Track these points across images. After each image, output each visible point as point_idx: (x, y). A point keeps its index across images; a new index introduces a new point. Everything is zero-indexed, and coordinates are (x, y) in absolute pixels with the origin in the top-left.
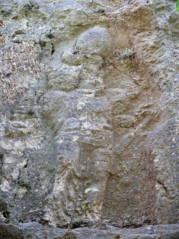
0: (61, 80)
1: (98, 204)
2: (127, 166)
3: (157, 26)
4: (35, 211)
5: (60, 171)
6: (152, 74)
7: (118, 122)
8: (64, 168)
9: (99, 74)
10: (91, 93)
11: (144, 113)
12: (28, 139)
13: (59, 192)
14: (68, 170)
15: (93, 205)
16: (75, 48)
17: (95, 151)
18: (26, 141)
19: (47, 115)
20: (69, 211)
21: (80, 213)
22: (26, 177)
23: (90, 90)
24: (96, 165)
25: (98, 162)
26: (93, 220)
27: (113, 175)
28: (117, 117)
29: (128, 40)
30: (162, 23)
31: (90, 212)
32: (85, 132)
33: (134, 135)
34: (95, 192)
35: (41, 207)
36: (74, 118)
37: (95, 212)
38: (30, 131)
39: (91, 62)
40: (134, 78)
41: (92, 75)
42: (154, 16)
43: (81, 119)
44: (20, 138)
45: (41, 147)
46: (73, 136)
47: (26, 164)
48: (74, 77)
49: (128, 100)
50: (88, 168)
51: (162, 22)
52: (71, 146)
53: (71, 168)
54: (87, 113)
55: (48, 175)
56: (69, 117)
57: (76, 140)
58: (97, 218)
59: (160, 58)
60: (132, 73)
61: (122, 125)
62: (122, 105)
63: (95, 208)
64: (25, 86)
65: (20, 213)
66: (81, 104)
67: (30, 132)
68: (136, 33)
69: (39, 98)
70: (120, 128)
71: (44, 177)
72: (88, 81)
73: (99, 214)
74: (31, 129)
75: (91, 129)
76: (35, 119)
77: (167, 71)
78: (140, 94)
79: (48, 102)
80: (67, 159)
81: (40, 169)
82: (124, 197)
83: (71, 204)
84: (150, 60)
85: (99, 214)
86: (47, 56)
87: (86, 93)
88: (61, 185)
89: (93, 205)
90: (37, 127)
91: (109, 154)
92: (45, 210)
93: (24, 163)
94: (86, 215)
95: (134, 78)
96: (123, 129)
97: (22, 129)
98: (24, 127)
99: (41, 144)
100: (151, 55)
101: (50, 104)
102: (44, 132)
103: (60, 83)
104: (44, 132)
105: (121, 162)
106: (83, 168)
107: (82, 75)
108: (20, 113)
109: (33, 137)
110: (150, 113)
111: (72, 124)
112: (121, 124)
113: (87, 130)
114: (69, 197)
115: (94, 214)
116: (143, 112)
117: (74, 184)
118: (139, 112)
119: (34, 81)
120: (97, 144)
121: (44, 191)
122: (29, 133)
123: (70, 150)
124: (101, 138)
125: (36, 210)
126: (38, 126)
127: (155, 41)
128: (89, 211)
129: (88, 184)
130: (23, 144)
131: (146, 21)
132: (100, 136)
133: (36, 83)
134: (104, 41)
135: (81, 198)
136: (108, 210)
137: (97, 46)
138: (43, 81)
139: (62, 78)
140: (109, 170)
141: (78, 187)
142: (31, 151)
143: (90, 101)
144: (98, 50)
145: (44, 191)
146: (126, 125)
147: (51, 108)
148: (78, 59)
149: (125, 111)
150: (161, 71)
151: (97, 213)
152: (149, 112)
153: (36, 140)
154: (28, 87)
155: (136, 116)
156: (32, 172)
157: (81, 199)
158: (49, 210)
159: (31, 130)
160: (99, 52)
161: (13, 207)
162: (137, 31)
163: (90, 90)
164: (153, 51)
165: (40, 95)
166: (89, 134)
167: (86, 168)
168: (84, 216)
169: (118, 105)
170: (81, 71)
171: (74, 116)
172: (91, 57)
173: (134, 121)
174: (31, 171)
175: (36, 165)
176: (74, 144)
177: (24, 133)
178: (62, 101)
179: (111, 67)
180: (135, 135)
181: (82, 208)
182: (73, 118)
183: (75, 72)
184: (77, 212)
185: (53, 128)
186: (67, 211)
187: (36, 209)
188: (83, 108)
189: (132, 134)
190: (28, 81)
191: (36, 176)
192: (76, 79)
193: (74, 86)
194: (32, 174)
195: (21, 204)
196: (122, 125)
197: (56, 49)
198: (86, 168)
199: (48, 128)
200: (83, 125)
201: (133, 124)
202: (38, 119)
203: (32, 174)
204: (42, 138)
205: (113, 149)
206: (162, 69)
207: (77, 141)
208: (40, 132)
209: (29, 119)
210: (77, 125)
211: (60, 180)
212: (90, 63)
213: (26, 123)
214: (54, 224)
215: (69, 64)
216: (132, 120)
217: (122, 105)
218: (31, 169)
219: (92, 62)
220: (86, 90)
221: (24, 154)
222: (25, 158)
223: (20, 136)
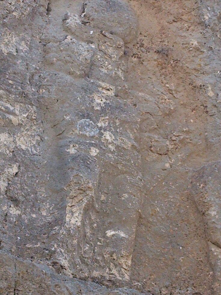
1: (128, 256)
2: (162, 209)
4: (36, 246)
5: (75, 195)
6: (195, 87)
8: (82, 192)
9: (120, 64)
10: (108, 90)
11: (184, 139)
12: (19, 135)
13: (75, 226)
14: (87, 197)
15: (121, 257)
16: (82, 16)
17: (119, 176)
18: (15, 136)
19: (46, 104)
20: (86, 258)
21: (102, 264)
23: (108, 85)
24: (123, 198)
25: (125, 194)
27: (142, 219)
28: (146, 134)
29: (160, 28)
30: (209, 18)
31: (116, 266)
32: (107, 146)
33: (170, 167)
35: (44, 243)
36: (91, 120)
38: (21, 123)
40: (168, 85)
41: (110, 64)
42: (199, 5)
43: (99, 125)
44: (6, 128)
45: (37, 151)
46: (92, 148)
47: (17, 171)
49: (161, 114)
50: (110, 200)
54: (107, 117)
55: (50, 196)
57: (95, 154)
58: (127, 277)
59: (207, 68)
60: (164, 77)
61: (152, 149)
62: (153, 119)
63: (122, 261)
64: (11, 50)
66: (99, 101)
68: (172, 21)
69: (33, 75)
70: (150, 153)
71: (44, 197)
72: (104, 71)
73: (128, 271)
74: (23, 119)
75: (115, 144)
76: (30, 106)
78: (175, 111)
81: (37, 184)
83: (87, 248)
84: (193, 67)
85: (128, 271)
86: (41, 14)
87: (103, 88)
88: (76, 217)
89: (121, 257)
91: (139, 187)
92: (53, 249)
93: (15, 170)
94: (110, 270)
95: (168, 85)
96: (154, 155)
97: (11, 117)
98: (14, 114)
99: (36, 146)
101: (53, 89)
102: (41, 129)
103: (67, 62)
104: (41, 129)
106: (103, 198)
107: (96, 59)
108: (7, 90)
109: (26, 132)
110: (191, 142)
112: (151, 147)
113: (110, 143)
114: (85, 236)
115: (123, 270)
116: (182, 137)
118: (176, 136)
119: (23, 47)
120: (124, 168)
122: (20, 125)
124: (129, 161)
125: (38, 246)
126: (33, 118)
127: (200, 40)
128: (114, 264)
130: (12, 139)
131: (186, 9)
132: (128, 157)
133: (26, 51)
135: (101, 242)
136: (137, 269)
137: (119, 23)
138: (37, 51)
139: (70, 56)
140: (140, 211)
141: (95, 225)
142: (24, 153)
145: (46, 219)
146: (158, 150)
147: (54, 96)
148: (91, 33)
149: (155, 128)
150: (209, 85)
151: (125, 269)
152: (191, 140)
153: (29, 139)
154: (16, 53)
157: (100, 244)
158: (63, 251)
159: (23, 121)
160: (121, 33)
161: (6, 233)
163: (107, 86)
164: (196, 54)
165: (34, 71)
167: (107, 200)
168: (108, 270)
169: (148, 118)
170: (95, 54)
171: (88, 116)
172: (111, 38)
173: (170, 147)
174: (25, 184)
175: (32, 177)
176: (93, 160)
177: (12, 123)
178: (70, 90)
179: (135, 60)
180: (171, 167)
181: (103, 257)
182: (89, 120)
184: (97, 261)
186: (83, 257)
187: (113, 235)
189: (167, 165)
190: (15, 44)
191: (33, 194)
193: (85, 72)
194: (27, 190)
195: (14, 231)
196: (152, 149)
197: (53, 7)
198: (107, 200)
200: (104, 135)
201: (168, 151)
202: (34, 107)
203: (27, 190)
205: (142, 180)
206: (211, 84)
207: (96, 156)
208: (34, 127)
210: (94, 132)
211: (74, 209)
212: (107, 44)
213: (17, 109)
214: (69, 272)
216: (167, 145)
218: (25, 181)
219: (111, 44)
220: (103, 84)
221: (14, 155)
222: (16, 161)
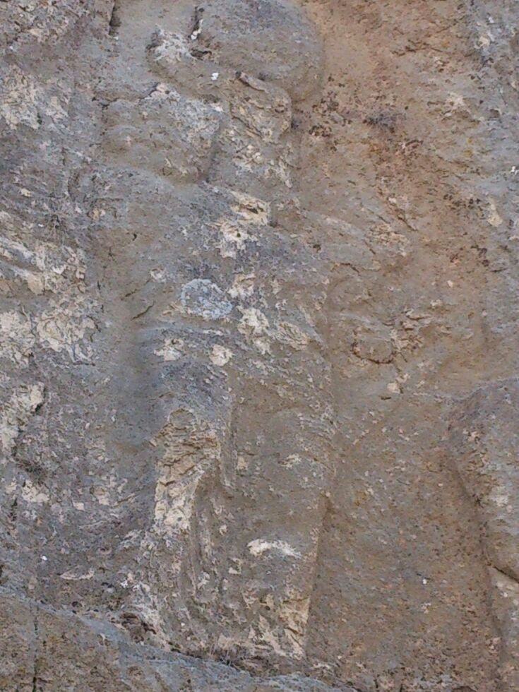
0: (159, 137)
3: (476, 47)
4: (83, 577)
5: (175, 457)
6: (457, 204)
7: (347, 334)
8: (191, 450)
10: (254, 211)
11: (431, 326)
12: (44, 316)
14: (205, 462)
19: (109, 244)
20: (201, 605)
21: (239, 619)
22: (45, 449)
23: (254, 200)
24: (289, 466)
25: (294, 456)
26: (283, 654)
27: (334, 513)
28: (344, 315)
29: (375, 65)
30: (491, 42)
34: (289, 556)
36: (213, 282)
37: (290, 626)
38: (50, 287)
39: (256, 103)
40: (393, 200)
41: (258, 150)
42: (468, 13)
44: (14, 301)
45: (86, 355)
46: (216, 347)
47: (39, 401)
48: (202, 139)
49: (378, 267)
50: (258, 469)
51: (493, 40)
52: (209, 378)
53: (213, 457)
55: (118, 460)
56: (195, 273)
57: (224, 362)
59: (486, 159)
60: (385, 181)
61: (358, 349)
62: (359, 280)
63: (287, 612)
64: (26, 118)
65: (438, 621)
66: (231, 237)
67: (51, 291)
68: (403, 49)
70: (353, 359)
72: (245, 165)
73: (302, 635)
74: (54, 280)
75: (271, 338)
76: (69, 249)
77: (512, 207)
78: (411, 259)
79: (113, 200)
80: (202, 421)
81: (88, 432)
82: (372, 595)
83: (204, 582)
85: (302, 635)
86: (97, 34)
87: (242, 207)
88: (179, 508)
89: (284, 602)
90: (75, 280)
91: (327, 439)
93: (35, 398)
94: (259, 633)
95: (393, 200)
96: (362, 363)
97: (26, 274)
98: (33, 268)
99: (85, 341)
100: (456, 137)
101: (125, 209)
102: (96, 304)
103: (156, 146)
104: (96, 304)
105: (358, 476)
106: (242, 463)
107: (226, 139)
109: (60, 310)
110: (448, 332)
111: (207, 304)
112: (354, 345)
113: (258, 336)
116: (427, 322)
117: (212, 513)
120: (290, 394)
121: (107, 513)
122: (47, 293)
123: (209, 394)
124: (303, 377)
125: (88, 577)
127: (469, 95)
128: (268, 619)
129: (259, 523)
130: (27, 326)
131: (438, 21)
132: (300, 369)
133: (61, 121)
134: (302, 45)
135: (236, 569)
136: (323, 630)
137: (279, 54)
139: (164, 132)
140: (328, 494)
141: (224, 527)
142: (56, 360)
143: (258, 237)
144: (283, 68)
145: (107, 513)
146: (371, 351)
147: (126, 226)
148: (214, 78)
149: (365, 301)
150: (490, 200)
151: (294, 632)
152: (448, 329)
153: (69, 326)
154: (38, 125)
155: (407, 330)
156: (64, 436)
157: (236, 572)
159: (53, 284)
162: (407, 44)
164: (461, 127)
165: (79, 166)
166: (267, 353)
167: (252, 468)
168: (253, 632)
169: (347, 278)
170: (222, 126)
173: (400, 345)
174: (60, 432)
175: (76, 415)
176: (218, 375)
177: (29, 290)
178: (164, 211)
180: (402, 392)
181: (243, 603)
182: (208, 281)
183: (202, 121)
184: (227, 612)
185: (128, 295)
188: (241, 258)
189: (393, 388)
190: (36, 103)
192: (206, 149)
194: (63, 445)
196: (358, 349)
197: (123, 17)
198: (252, 468)
199: (112, 295)
200: (245, 317)
201: (394, 354)
204: (91, 325)
205: (335, 423)
206: (495, 197)
208: (80, 299)
209: (50, 245)
210: (221, 311)
211: (174, 491)
212: (252, 104)
214: (162, 639)
215: (181, 87)
216: (393, 340)
217: (359, 280)
218: (58, 425)
219: (260, 102)
220: (242, 198)
221: (33, 364)
222: (38, 379)
223: (15, 296)
